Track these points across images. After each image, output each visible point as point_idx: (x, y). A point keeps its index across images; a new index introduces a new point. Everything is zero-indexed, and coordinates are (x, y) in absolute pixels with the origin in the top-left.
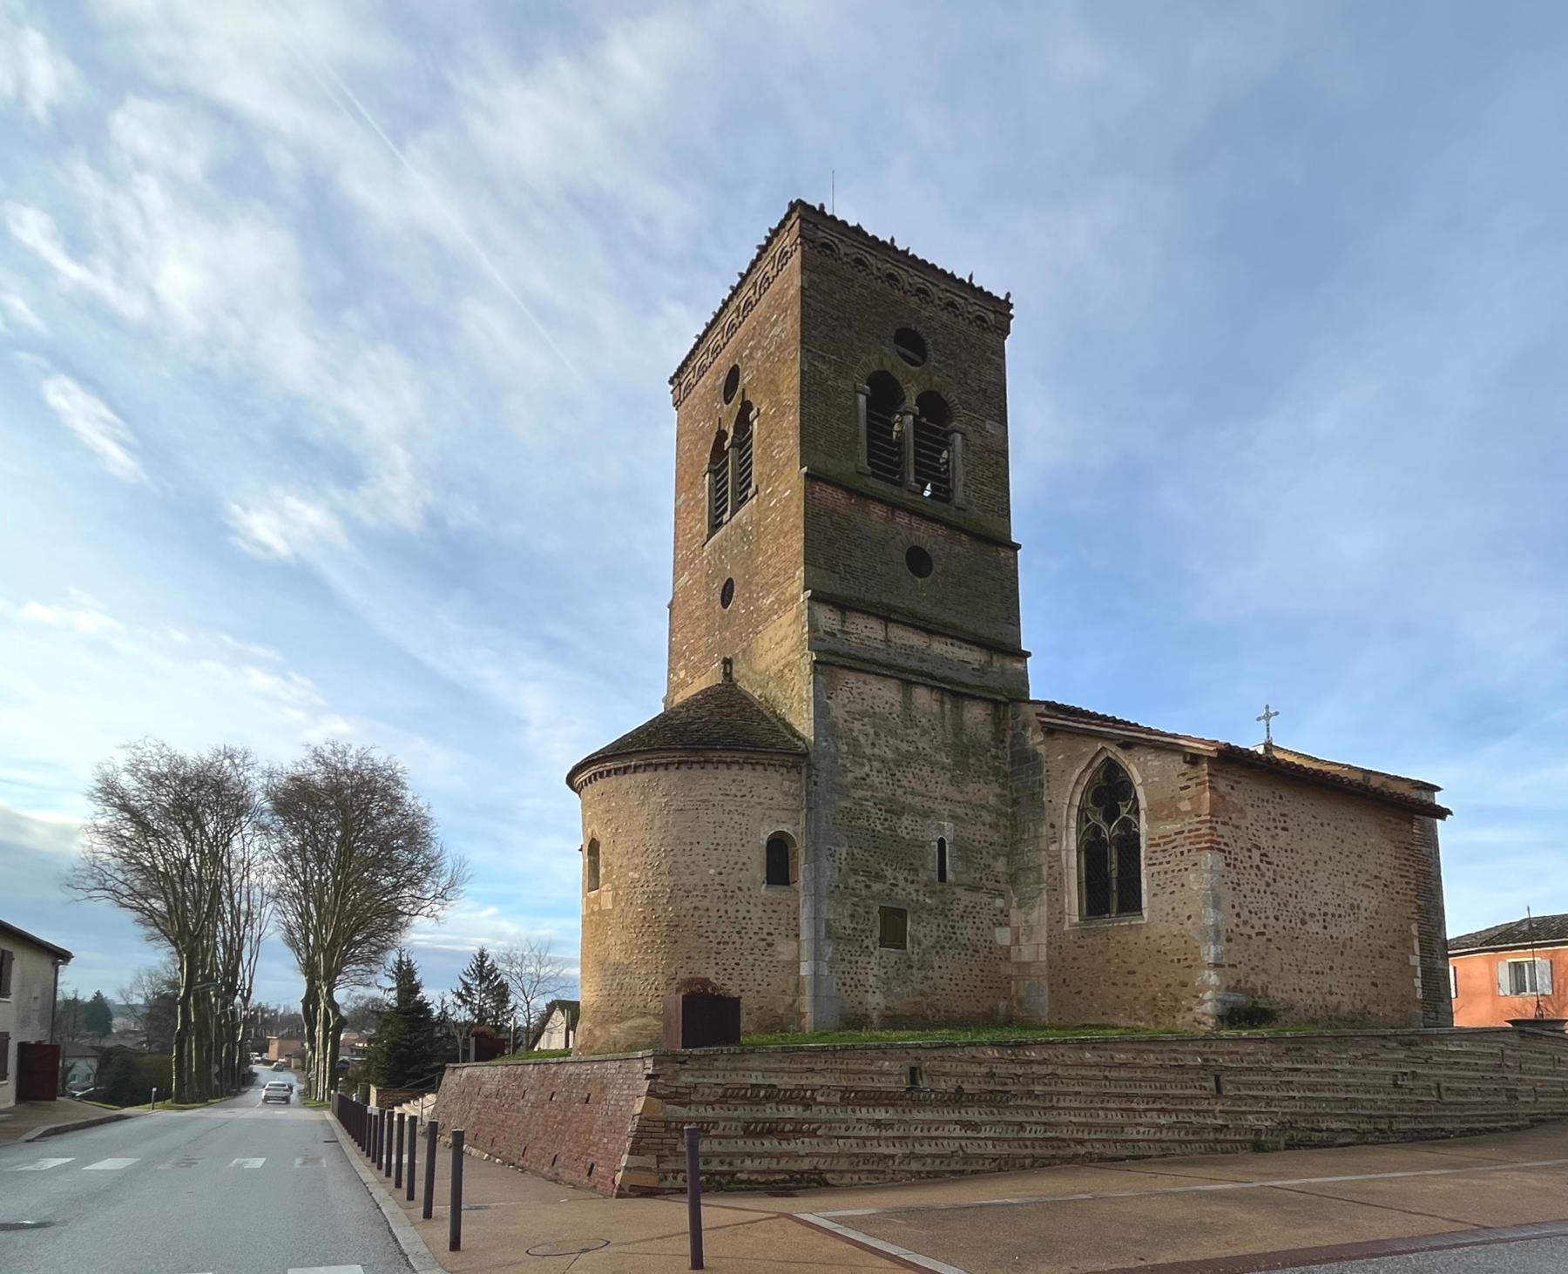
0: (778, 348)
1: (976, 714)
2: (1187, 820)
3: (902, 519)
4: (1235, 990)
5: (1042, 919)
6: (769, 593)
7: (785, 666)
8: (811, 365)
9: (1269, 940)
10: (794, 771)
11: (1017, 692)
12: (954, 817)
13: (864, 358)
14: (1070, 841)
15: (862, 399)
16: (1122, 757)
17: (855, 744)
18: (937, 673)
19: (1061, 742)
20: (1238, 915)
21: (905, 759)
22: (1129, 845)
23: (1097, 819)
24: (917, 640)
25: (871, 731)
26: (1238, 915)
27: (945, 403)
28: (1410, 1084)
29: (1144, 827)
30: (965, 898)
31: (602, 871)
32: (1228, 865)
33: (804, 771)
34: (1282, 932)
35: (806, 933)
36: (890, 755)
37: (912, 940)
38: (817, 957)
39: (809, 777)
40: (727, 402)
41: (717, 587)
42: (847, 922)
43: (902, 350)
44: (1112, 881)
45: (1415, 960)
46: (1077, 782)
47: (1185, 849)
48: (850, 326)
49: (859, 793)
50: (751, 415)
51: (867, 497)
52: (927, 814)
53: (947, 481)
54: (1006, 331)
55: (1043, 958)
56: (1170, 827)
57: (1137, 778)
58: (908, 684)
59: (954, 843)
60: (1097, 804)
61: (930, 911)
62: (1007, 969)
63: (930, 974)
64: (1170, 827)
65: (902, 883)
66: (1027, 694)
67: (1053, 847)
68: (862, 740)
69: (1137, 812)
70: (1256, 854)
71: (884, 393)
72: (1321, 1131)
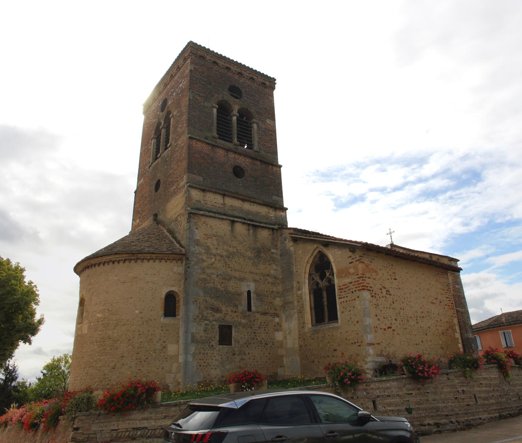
0: (181, 91)
1: (264, 234)
2: (353, 277)
3: (231, 155)
4: (381, 355)
5: (292, 328)
6: (173, 185)
7: (178, 215)
8: (193, 97)
9: (394, 330)
10: (179, 262)
11: (282, 224)
12: (255, 281)
13: (216, 95)
14: (306, 289)
15: (215, 110)
16: (325, 251)
17: (208, 249)
18: (261, 221)
19: (301, 245)
20: (379, 319)
21: (231, 255)
22: (331, 288)
23: (317, 279)
24: (237, 203)
25: (216, 243)
26: (379, 319)
27: (250, 112)
28: (462, 396)
29: (336, 281)
30: (261, 319)
31: (85, 314)
32: (372, 296)
33: (184, 262)
34: (399, 326)
35: (181, 341)
36: (224, 254)
37: (235, 341)
38: (186, 352)
39: (186, 264)
40: (162, 111)
41: (154, 182)
42: (202, 333)
43: (232, 93)
44: (325, 308)
45: (458, 335)
46: (307, 262)
47: (353, 290)
48: (210, 84)
49: (208, 271)
50: (170, 116)
51: (216, 146)
52: (242, 279)
53: (251, 141)
54: (274, 88)
55: (297, 346)
56: (347, 280)
57: (332, 259)
58: (233, 222)
59: (255, 292)
60: (317, 272)
61: (244, 326)
62: (281, 352)
63: (244, 357)
64: (347, 280)
65: (230, 313)
66: (287, 226)
67: (299, 292)
68: (211, 247)
69: (333, 275)
70: (384, 291)
71: (224, 110)
72: (425, 426)
